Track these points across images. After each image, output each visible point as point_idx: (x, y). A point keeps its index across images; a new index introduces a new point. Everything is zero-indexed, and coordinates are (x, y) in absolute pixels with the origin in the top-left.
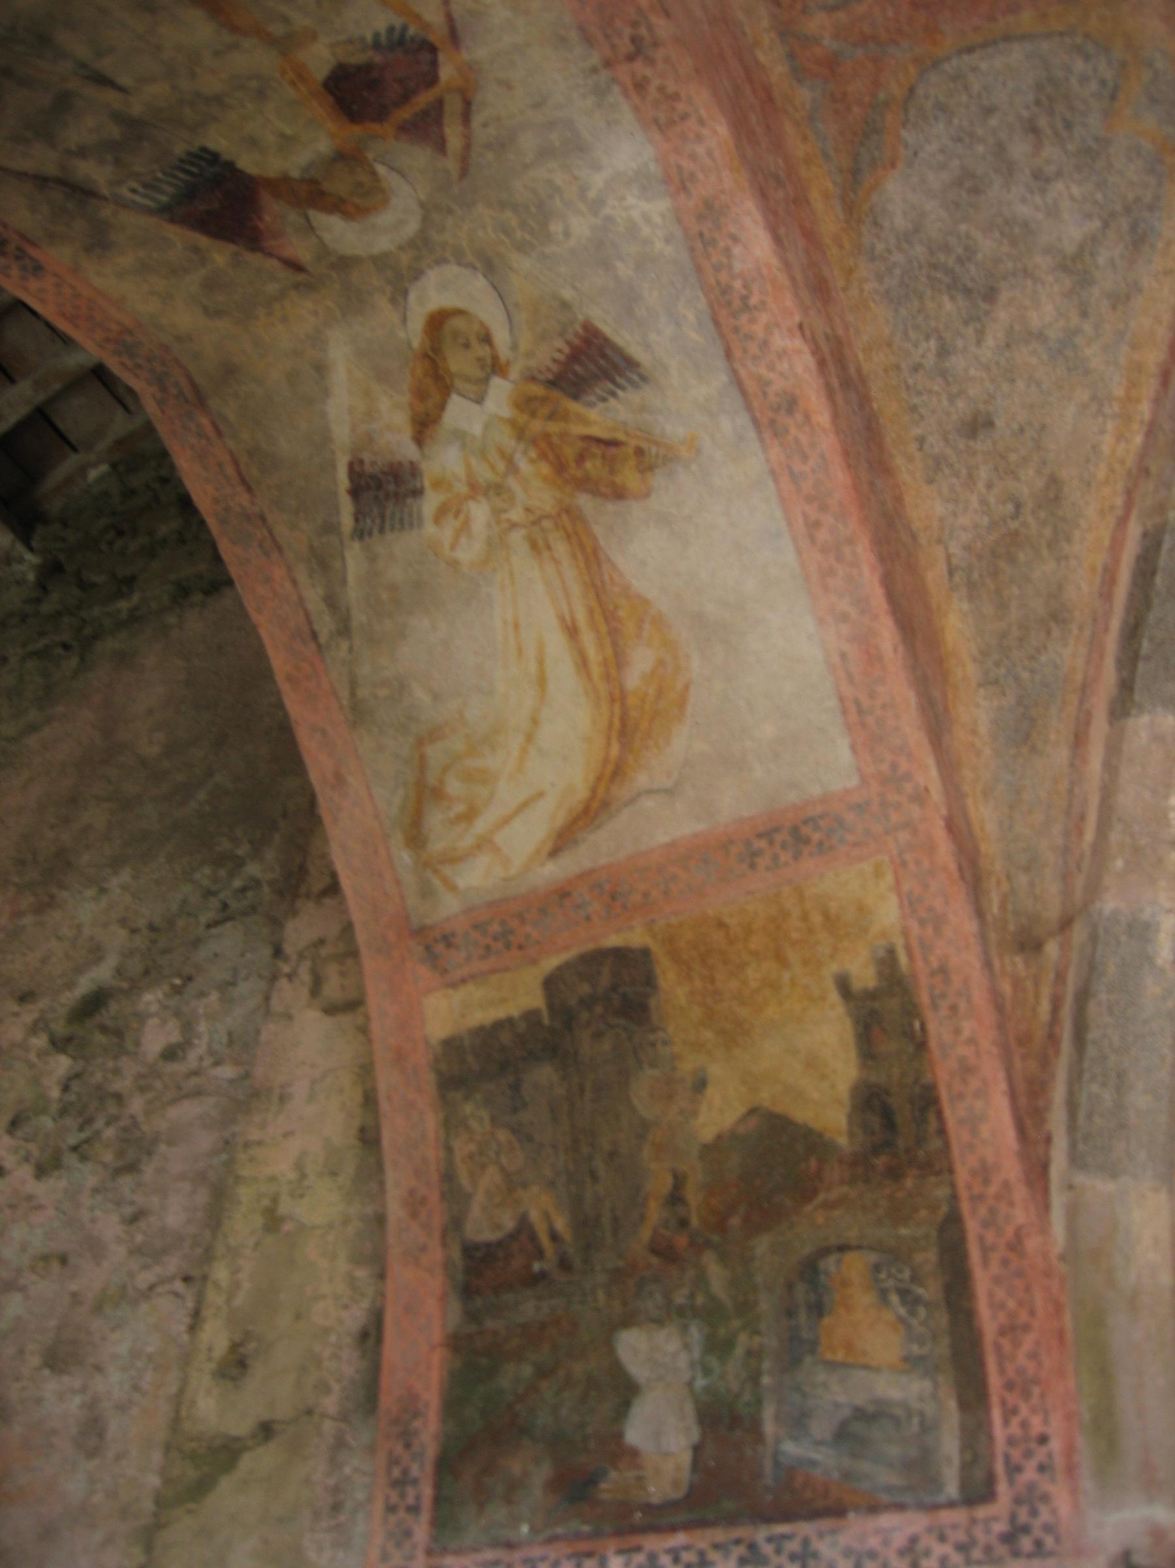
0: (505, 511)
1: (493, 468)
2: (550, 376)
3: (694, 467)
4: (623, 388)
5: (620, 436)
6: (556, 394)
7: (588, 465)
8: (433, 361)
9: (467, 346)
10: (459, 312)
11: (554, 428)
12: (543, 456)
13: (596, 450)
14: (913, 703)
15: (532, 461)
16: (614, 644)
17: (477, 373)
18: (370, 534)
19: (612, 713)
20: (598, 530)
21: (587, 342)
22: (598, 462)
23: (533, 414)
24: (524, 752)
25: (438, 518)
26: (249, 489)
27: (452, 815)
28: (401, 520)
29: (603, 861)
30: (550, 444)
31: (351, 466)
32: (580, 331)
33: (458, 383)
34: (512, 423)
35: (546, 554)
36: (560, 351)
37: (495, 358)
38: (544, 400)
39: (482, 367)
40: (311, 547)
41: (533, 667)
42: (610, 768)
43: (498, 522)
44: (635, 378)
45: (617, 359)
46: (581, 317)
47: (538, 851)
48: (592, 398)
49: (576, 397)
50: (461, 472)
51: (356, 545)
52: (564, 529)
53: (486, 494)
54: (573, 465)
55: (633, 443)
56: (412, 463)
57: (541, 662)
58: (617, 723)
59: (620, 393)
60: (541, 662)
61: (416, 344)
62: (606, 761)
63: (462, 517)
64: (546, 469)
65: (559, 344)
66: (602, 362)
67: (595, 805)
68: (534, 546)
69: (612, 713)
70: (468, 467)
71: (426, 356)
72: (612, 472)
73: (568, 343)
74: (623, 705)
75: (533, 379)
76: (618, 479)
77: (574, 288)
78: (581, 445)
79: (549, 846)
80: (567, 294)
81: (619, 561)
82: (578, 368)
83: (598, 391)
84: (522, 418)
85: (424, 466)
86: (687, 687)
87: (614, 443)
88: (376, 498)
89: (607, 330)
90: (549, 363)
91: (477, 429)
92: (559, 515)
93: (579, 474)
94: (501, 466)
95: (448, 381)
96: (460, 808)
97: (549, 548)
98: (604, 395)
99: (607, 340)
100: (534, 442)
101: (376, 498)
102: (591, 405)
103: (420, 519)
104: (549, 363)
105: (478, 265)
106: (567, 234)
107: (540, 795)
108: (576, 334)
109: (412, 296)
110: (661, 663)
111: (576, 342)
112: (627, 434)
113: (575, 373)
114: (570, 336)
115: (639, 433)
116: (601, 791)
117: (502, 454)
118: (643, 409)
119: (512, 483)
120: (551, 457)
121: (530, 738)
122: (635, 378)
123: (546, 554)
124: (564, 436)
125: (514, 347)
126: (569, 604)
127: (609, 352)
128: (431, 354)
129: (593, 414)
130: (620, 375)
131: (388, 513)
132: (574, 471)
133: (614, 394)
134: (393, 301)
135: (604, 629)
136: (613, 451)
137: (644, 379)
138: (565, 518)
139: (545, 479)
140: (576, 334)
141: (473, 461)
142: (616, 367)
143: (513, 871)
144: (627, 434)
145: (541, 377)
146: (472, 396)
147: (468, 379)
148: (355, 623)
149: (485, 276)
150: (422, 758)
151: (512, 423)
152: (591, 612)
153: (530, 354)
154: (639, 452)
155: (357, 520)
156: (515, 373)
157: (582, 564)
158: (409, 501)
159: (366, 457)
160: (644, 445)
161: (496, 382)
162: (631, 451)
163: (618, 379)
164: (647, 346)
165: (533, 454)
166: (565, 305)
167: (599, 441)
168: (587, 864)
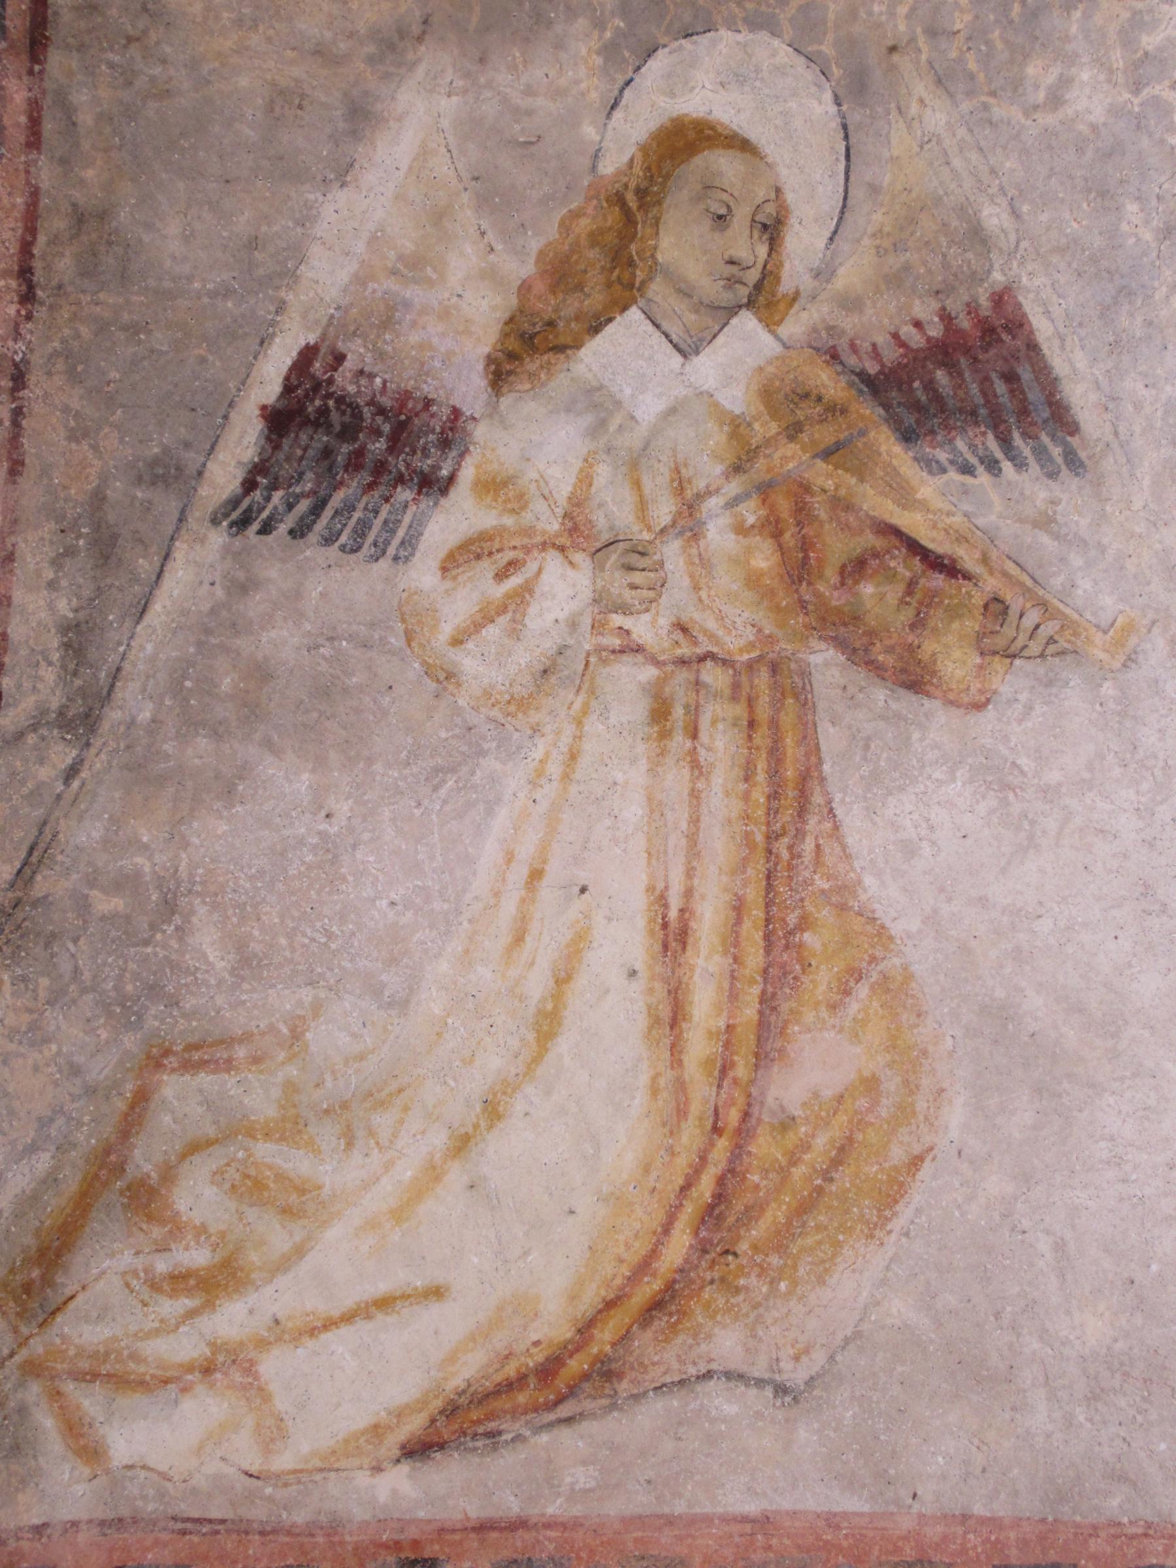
0: (625, 609)
1: (642, 506)
2: (872, 368)
3: (1108, 689)
4: (1020, 465)
5: (968, 560)
6: (867, 410)
7: (868, 589)
8: (629, 219)
9: (721, 220)
10: (743, 145)
11: (823, 476)
12: (773, 528)
13: (902, 566)
14: (611, 1324)
15: (741, 529)
16: (767, 1001)
17: (711, 289)
18: (266, 529)
19: (703, 1159)
20: (830, 738)
21: (988, 332)
22: (894, 593)
23: (793, 431)
24: (432, 1174)
25: (450, 564)
26: (28, 297)
27: (162, 1266)
28: (361, 530)
29: (554, 1508)
30: (802, 511)
31: (308, 354)
32: (984, 302)
33: (657, 289)
34: (736, 427)
35: (679, 741)
36: (918, 324)
37: (769, 276)
38: (835, 410)
39: (732, 282)
40: (98, 499)
41: (537, 985)
42: (651, 1287)
43: (598, 627)
44: (1056, 451)
45: (1034, 395)
46: (997, 276)
47: (376, 1431)
48: (942, 456)
49: (908, 437)
50: (563, 486)
51: (218, 538)
52: (751, 703)
53: (598, 552)
54: (831, 574)
55: (991, 584)
56: (456, 412)
57: (563, 979)
58: (706, 1187)
59: (1007, 466)
60: (563, 979)
61: (608, 167)
62: (645, 1266)
63: (515, 581)
64: (764, 558)
65: (924, 310)
66: (1000, 387)
67: (576, 1365)
68: (660, 713)
69: (703, 1159)
70: (585, 479)
71: (619, 200)
72: (917, 624)
73: (946, 317)
74: (738, 1150)
75: (834, 356)
76: (929, 647)
77: (1016, 214)
78: (870, 540)
79: (415, 1425)
80: (994, 217)
81: (852, 818)
82: (941, 376)
83: (960, 444)
84: (765, 428)
85: (480, 432)
86: (916, 1162)
87: (949, 568)
88: (327, 453)
89: (1042, 328)
90: (881, 339)
91: (649, 408)
92: (751, 666)
93: (837, 599)
94: (664, 511)
95: (640, 275)
96: (198, 1257)
97: (693, 733)
98: (974, 460)
99: (1033, 347)
100: (764, 490)
101: (327, 453)
102: (934, 467)
103: (410, 543)
104: (881, 339)
105: (836, 72)
106: (1055, 100)
107: (436, 1293)
108: (971, 308)
109: (657, 65)
110: (870, 1085)
111: (965, 323)
112: (985, 560)
113: (930, 386)
114: (955, 305)
115: (1011, 567)
116: (604, 1336)
117: (680, 485)
118: (1045, 522)
119: (672, 553)
120: (789, 538)
121: (462, 1144)
122: (1056, 451)
123: (679, 741)
124: (841, 504)
125: (823, 273)
126: (690, 873)
127: (1026, 374)
128: (633, 203)
129: (928, 488)
130: (1026, 435)
131: (338, 499)
132: (827, 587)
133: (992, 466)
134: (610, 51)
135: (755, 959)
136: (938, 580)
137: (1073, 461)
138: (763, 678)
139: (753, 580)
140: (971, 308)
141: (603, 472)
142: (1024, 411)
143: (284, 1461)
144: (985, 560)
145: (852, 361)
146: (676, 332)
147: (685, 292)
148: (113, 716)
149: (838, 102)
150: (142, 1097)
151: (736, 427)
152: (739, 908)
153: (850, 303)
154: (996, 608)
155: (249, 485)
156: (795, 326)
157: (759, 796)
158: (404, 494)
159: (356, 353)
160: (1016, 603)
161: (746, 322)
162: (978, 600)
163: (1017, 440)
164: (1110, 402)
165: (751, 513)
166: (977, 236)
167: (914, 547)
168: (511, 1505)
